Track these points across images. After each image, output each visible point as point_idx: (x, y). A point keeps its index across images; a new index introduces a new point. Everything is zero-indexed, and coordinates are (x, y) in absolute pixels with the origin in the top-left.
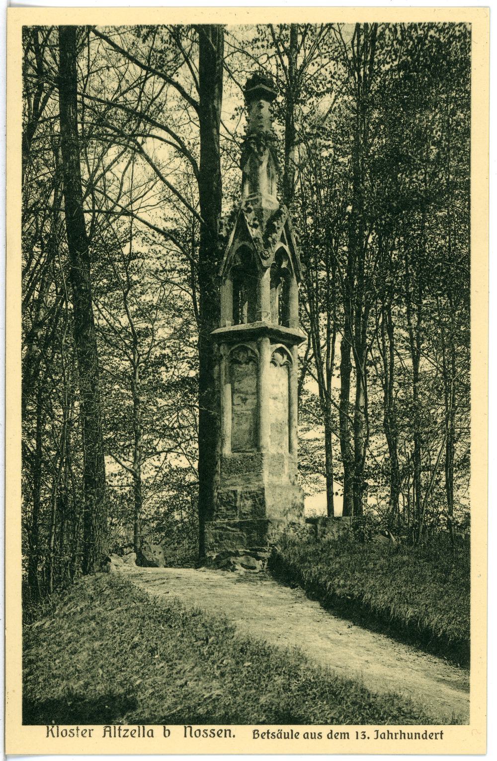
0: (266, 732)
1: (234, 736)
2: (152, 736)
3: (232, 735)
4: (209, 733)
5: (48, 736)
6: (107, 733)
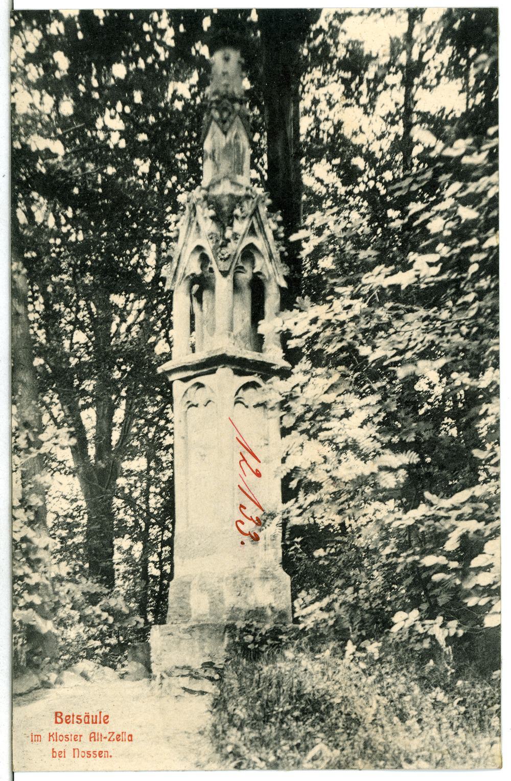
2: (131, 740)
6: (93, 739)
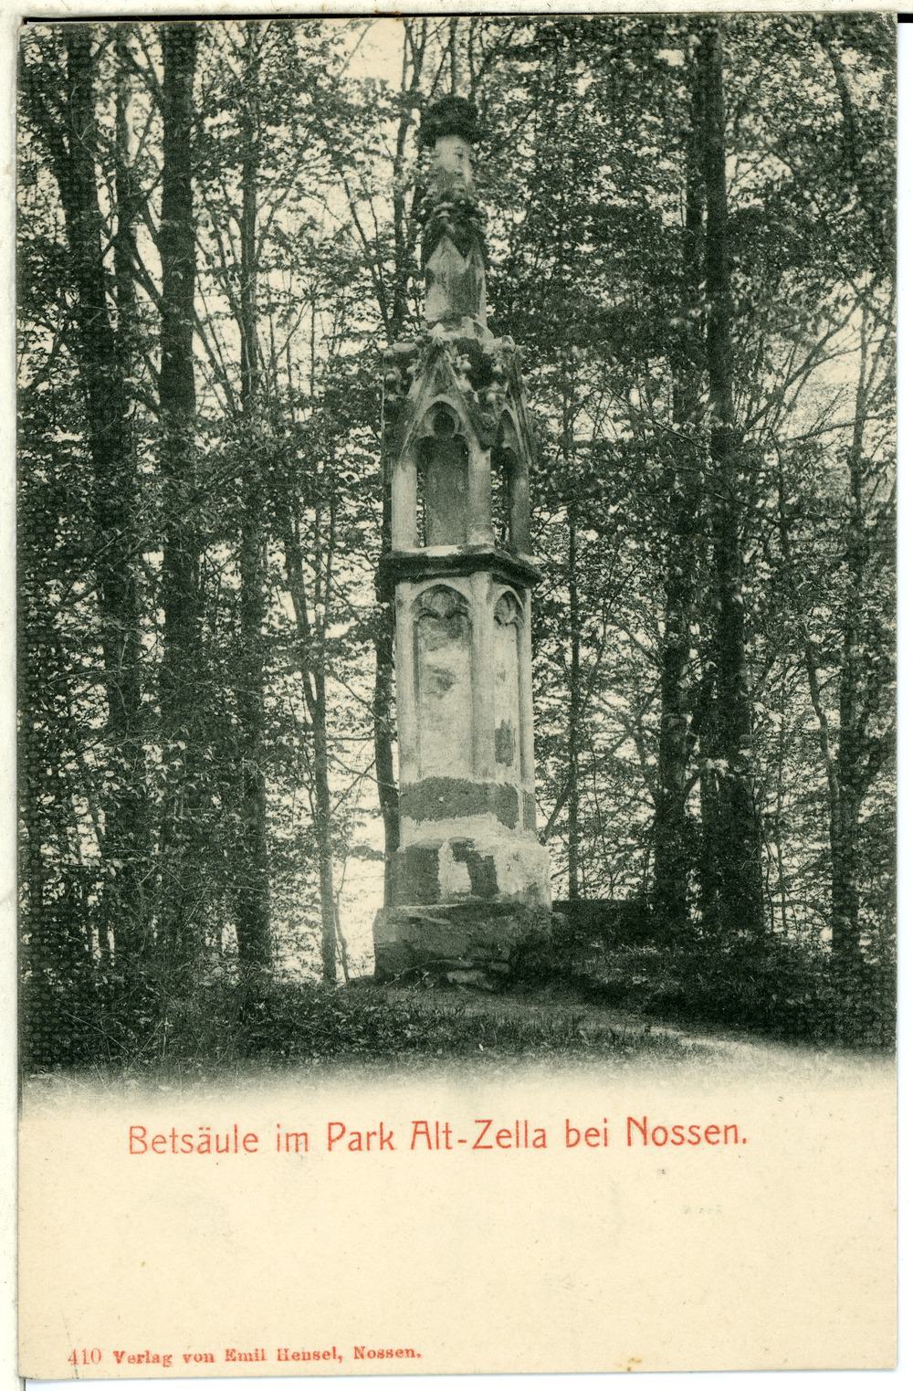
0: (167, 1134)
1: (744, 1141)
2: (544, 1145)
3: (740, 1139)
4: (685, 1133)
5: (645, 1119)
